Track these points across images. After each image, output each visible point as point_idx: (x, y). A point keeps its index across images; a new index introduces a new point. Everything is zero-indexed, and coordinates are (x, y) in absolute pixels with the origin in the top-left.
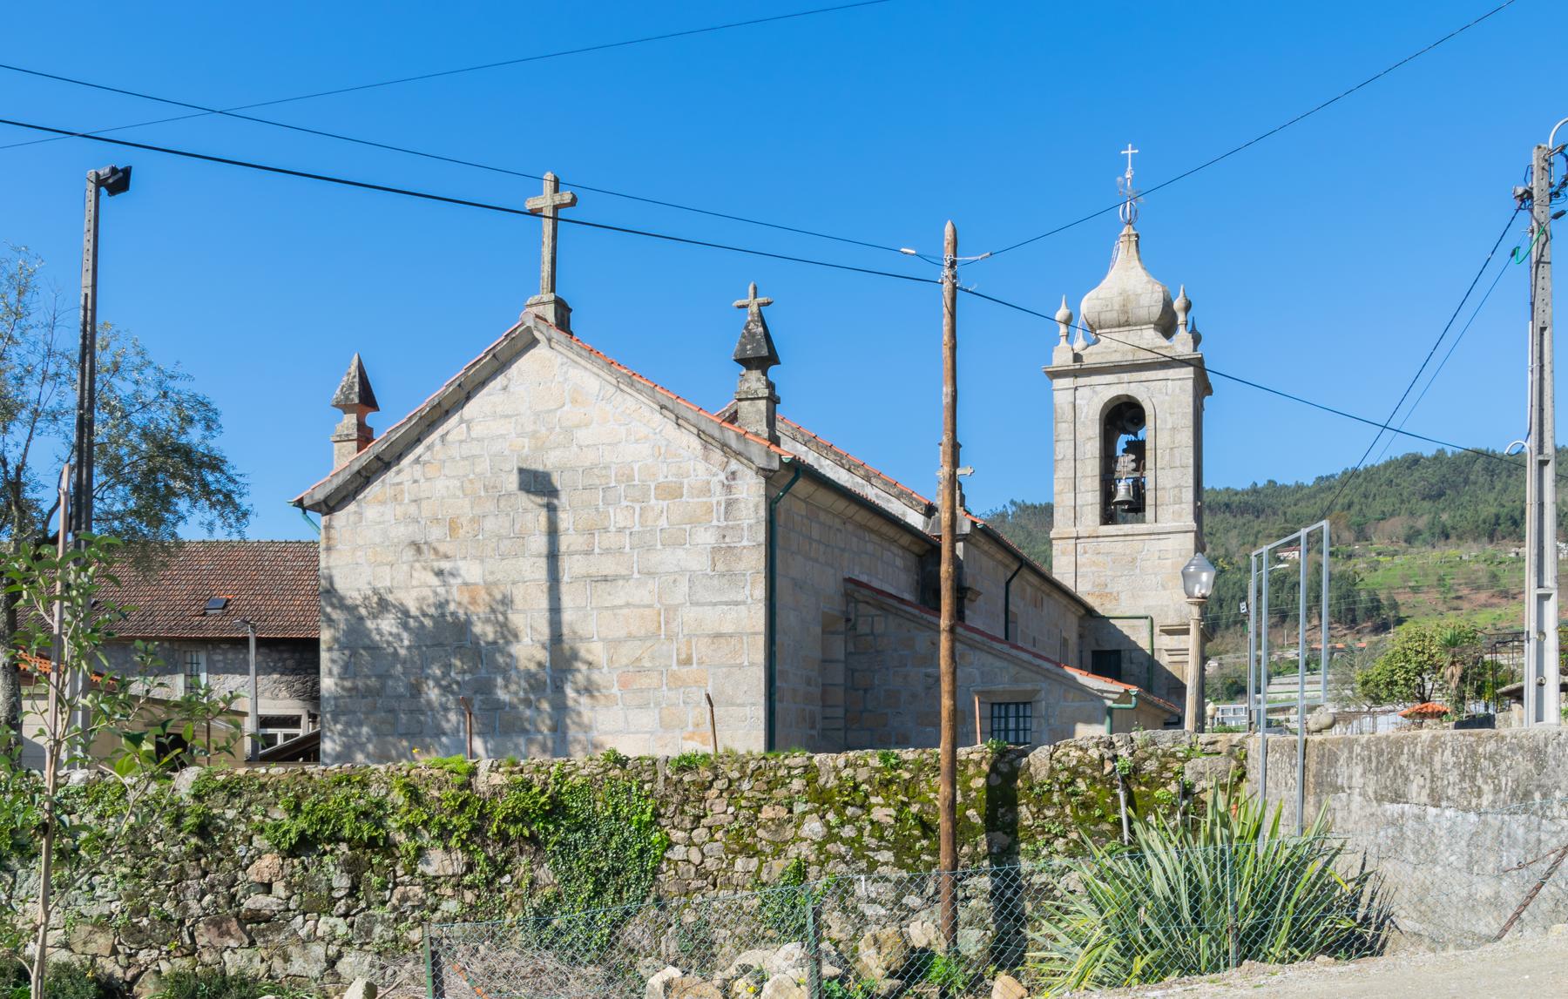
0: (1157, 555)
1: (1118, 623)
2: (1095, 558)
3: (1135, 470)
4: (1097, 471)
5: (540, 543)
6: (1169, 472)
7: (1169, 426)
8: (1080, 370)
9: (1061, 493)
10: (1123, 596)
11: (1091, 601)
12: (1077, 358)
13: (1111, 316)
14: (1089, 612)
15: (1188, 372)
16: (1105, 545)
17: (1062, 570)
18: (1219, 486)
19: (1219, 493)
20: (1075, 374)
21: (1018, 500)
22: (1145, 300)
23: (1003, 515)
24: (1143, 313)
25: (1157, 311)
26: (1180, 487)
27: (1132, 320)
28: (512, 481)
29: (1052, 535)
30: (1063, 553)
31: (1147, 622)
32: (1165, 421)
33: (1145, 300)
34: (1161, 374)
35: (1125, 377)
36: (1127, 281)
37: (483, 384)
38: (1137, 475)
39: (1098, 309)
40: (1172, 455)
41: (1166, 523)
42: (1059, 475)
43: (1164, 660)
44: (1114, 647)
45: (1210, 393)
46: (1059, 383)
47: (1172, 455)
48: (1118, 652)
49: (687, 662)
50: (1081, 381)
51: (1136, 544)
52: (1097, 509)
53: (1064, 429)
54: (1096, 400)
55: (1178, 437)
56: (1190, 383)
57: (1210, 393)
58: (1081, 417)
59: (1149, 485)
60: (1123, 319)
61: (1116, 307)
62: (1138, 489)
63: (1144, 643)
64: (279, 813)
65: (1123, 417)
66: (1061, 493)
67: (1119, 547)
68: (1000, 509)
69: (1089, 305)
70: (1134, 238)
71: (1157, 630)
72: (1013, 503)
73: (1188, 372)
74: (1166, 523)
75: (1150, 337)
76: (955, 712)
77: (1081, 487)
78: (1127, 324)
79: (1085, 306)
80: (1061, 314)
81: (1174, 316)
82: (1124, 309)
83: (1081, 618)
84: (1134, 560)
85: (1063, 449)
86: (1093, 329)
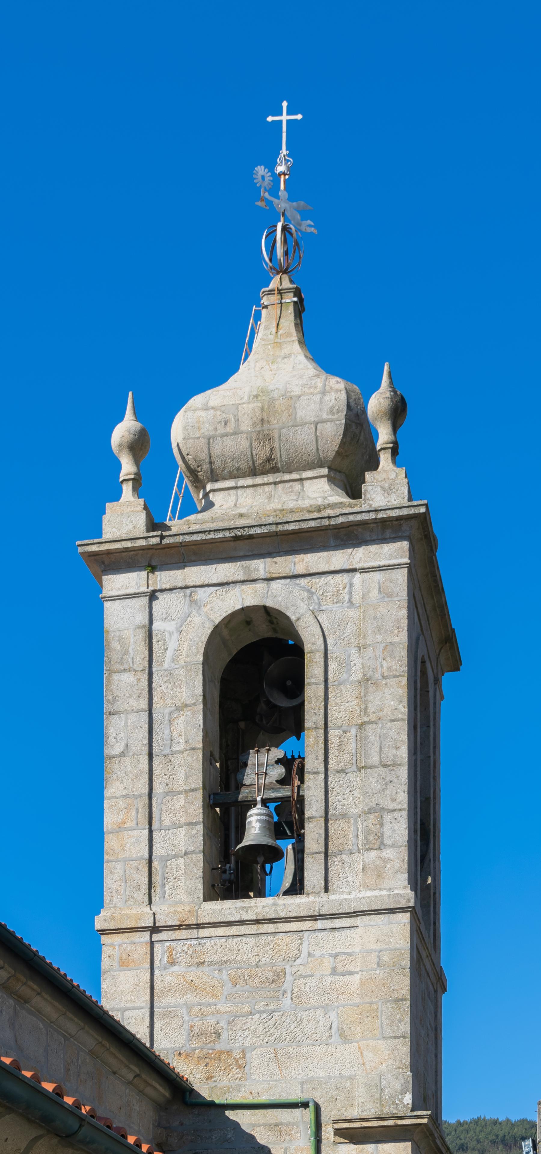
0: (328, 963)
1: (244, 1119)
2: (193, 974)
3: (283, 782)
4: (197, 780)
6: (355, 779)
7: (357, 675)
8: (159, 555)
9: (120, 829)
10: (255, 1058)
11: (182, 1068)
13: (234, 447)
14: (180, 1091)
15: (396, 552)
16: (216, 945)
17: (121, 995)
18: (467, 1117)
19: (513, 1125)
22: (307, 410)
24: (302, 439)
25: (333, 432)
26: (378, 811)
27: (281, 456)
29: (99, 923)
30: (124, 964)
31: (308, 1114)
32: (346, 665)
33: (307, 410)
34: (338, 558)
35: (260, 566)
36: (279, 379)
38: (284, 792)
39: (207, 429)
40: (361, 740)
42: (113, 790)
45: (456, 665)
46: (116, 583)
47: (361, 740)
50: (164, 578)
52: (196, 866)
53: (123, 687)
54: (197, 619)
55: (375, 700)
56: (401, 577)
57: (456, 665)
58: (165, 659)
59: (313, 808)
60: (261, 453)
61: (246, 426)
62: (288, 819)
66: (120, 829)
67: (246, 948)
69: (194, 423)
70: (290, 299)
71: (328, 1132)
73: (396, 552)
74: (349, 892)
75: (316, 495)
76: (417, 834)
77: (163, 817)
79: (180, 429)
81: (371, 437)
82: (264, 436)
83: (161, 1108)
84: (278, 977)
85: (123, 732)
86: (203, 475)
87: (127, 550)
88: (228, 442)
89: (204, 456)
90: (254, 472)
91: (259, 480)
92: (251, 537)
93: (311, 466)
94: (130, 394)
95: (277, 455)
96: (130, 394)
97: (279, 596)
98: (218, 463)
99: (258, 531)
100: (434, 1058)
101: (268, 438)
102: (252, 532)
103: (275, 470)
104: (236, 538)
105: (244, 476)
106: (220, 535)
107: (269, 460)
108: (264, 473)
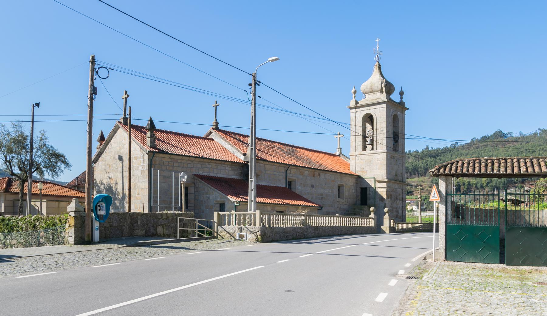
5: (120, 169)
12: (357, 103)
13: (368, 90)
20: (355, 108)
21: (542, 128)
22: (376, 85)
23: (536, 134)
24: (376, 89)
28: (117, 157)
34: (378, 106)
35: (369, 108)
37: (113, 136)
41: (379, 150)
43: (378, 190)
44: (365, 187)
48: (366, 188)
49: (138, 194)
50: (357, 110)
51: (371, 156)
59: (375, 139)
63: (373, 186)
64: (43, 224)
65: (369, 119)
68: (534, 132)
72: (539, 129)
74: (379, 150)
78: (372, 92)
80: (353, 91)
84: (371, 161)
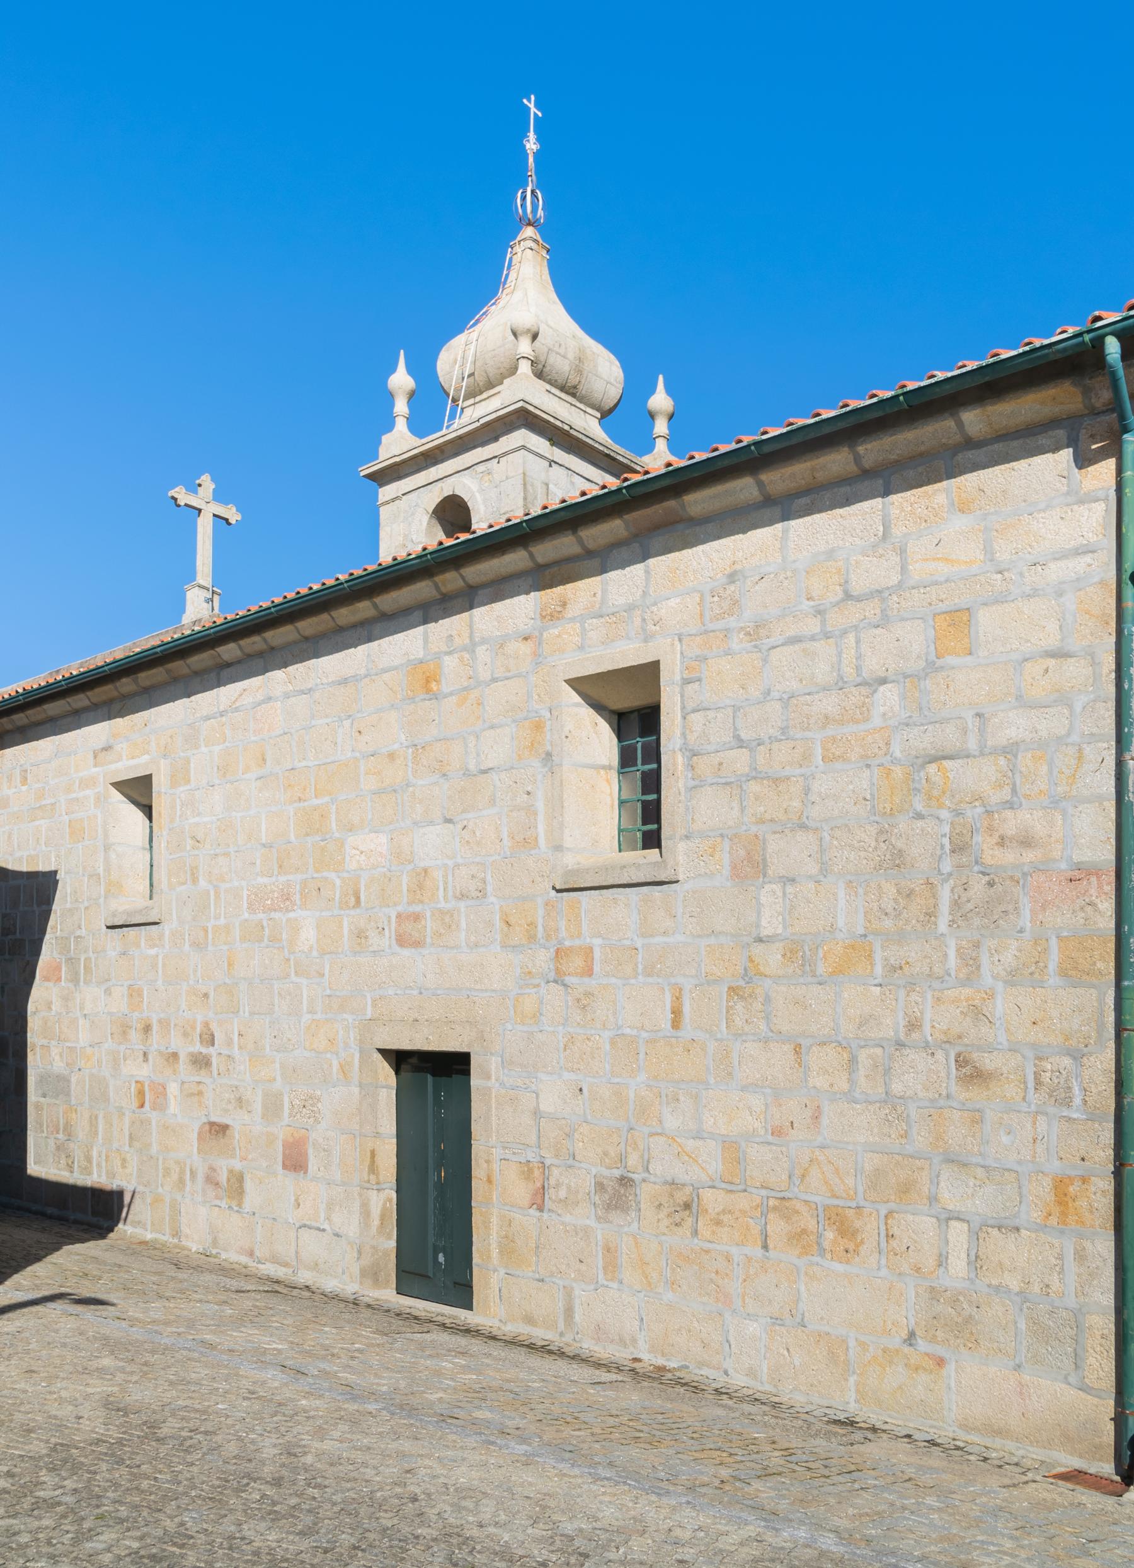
27: (583, 390)
60: (573, 380)
87: (548, 422)
88: (559, 358)
89: (542, 359)
90: (562, 389)
91: (563, 395)
92: (614, 459)
93: (593, 407)
94: (661, 378)
95: (580, 387)
96: (661, 378)
97: (420, 442)
98: (546, 370)
99: (621, 459)
100: (687, 1009)
101: (580, 372)
102: (618, 457)
103: (574, 395)
104: (608, 456)
105: (556, 387)
106: (601, 448)
107: (575, 387)
108: (567, 393)
